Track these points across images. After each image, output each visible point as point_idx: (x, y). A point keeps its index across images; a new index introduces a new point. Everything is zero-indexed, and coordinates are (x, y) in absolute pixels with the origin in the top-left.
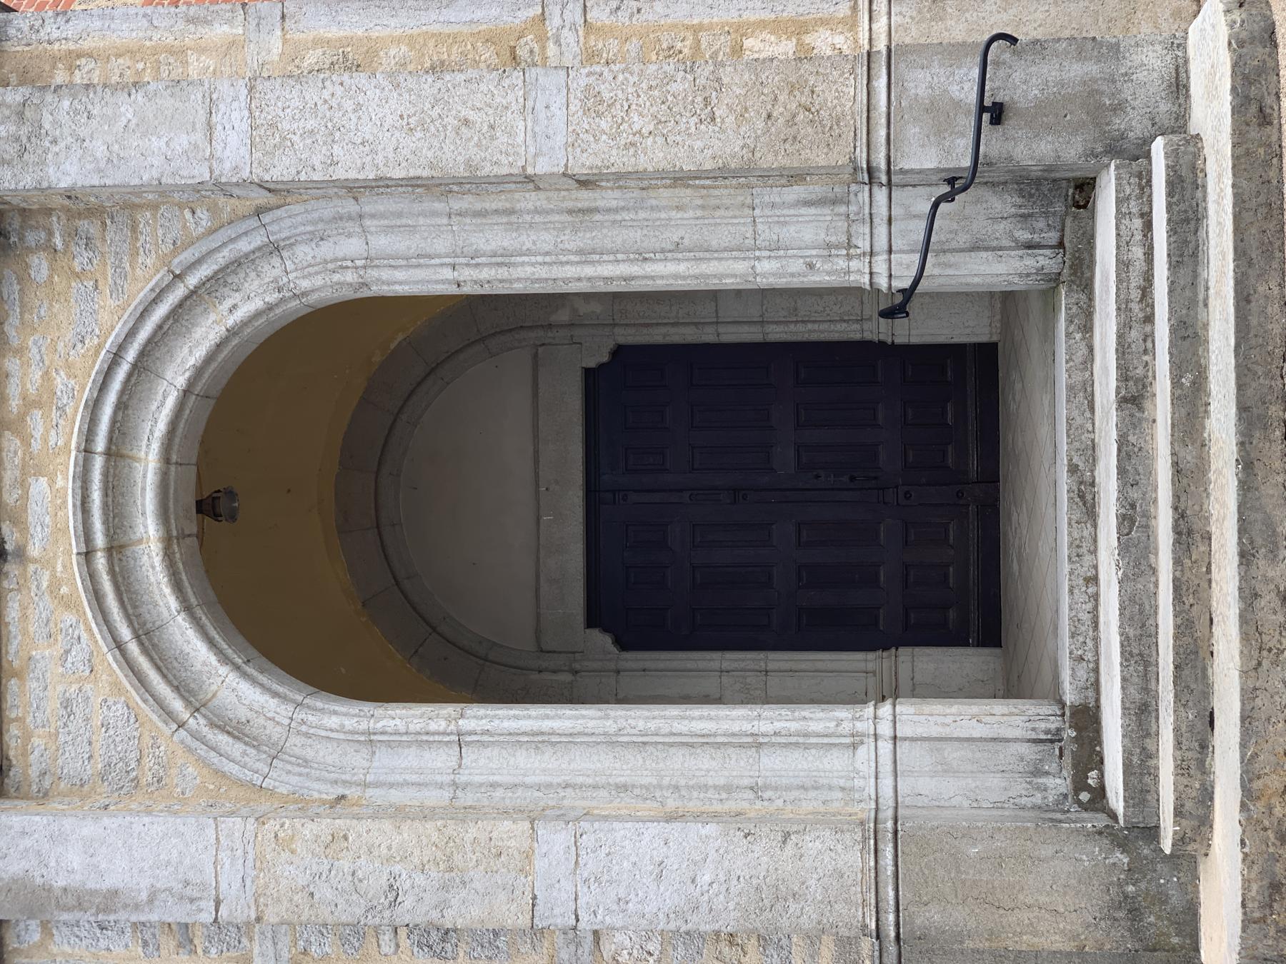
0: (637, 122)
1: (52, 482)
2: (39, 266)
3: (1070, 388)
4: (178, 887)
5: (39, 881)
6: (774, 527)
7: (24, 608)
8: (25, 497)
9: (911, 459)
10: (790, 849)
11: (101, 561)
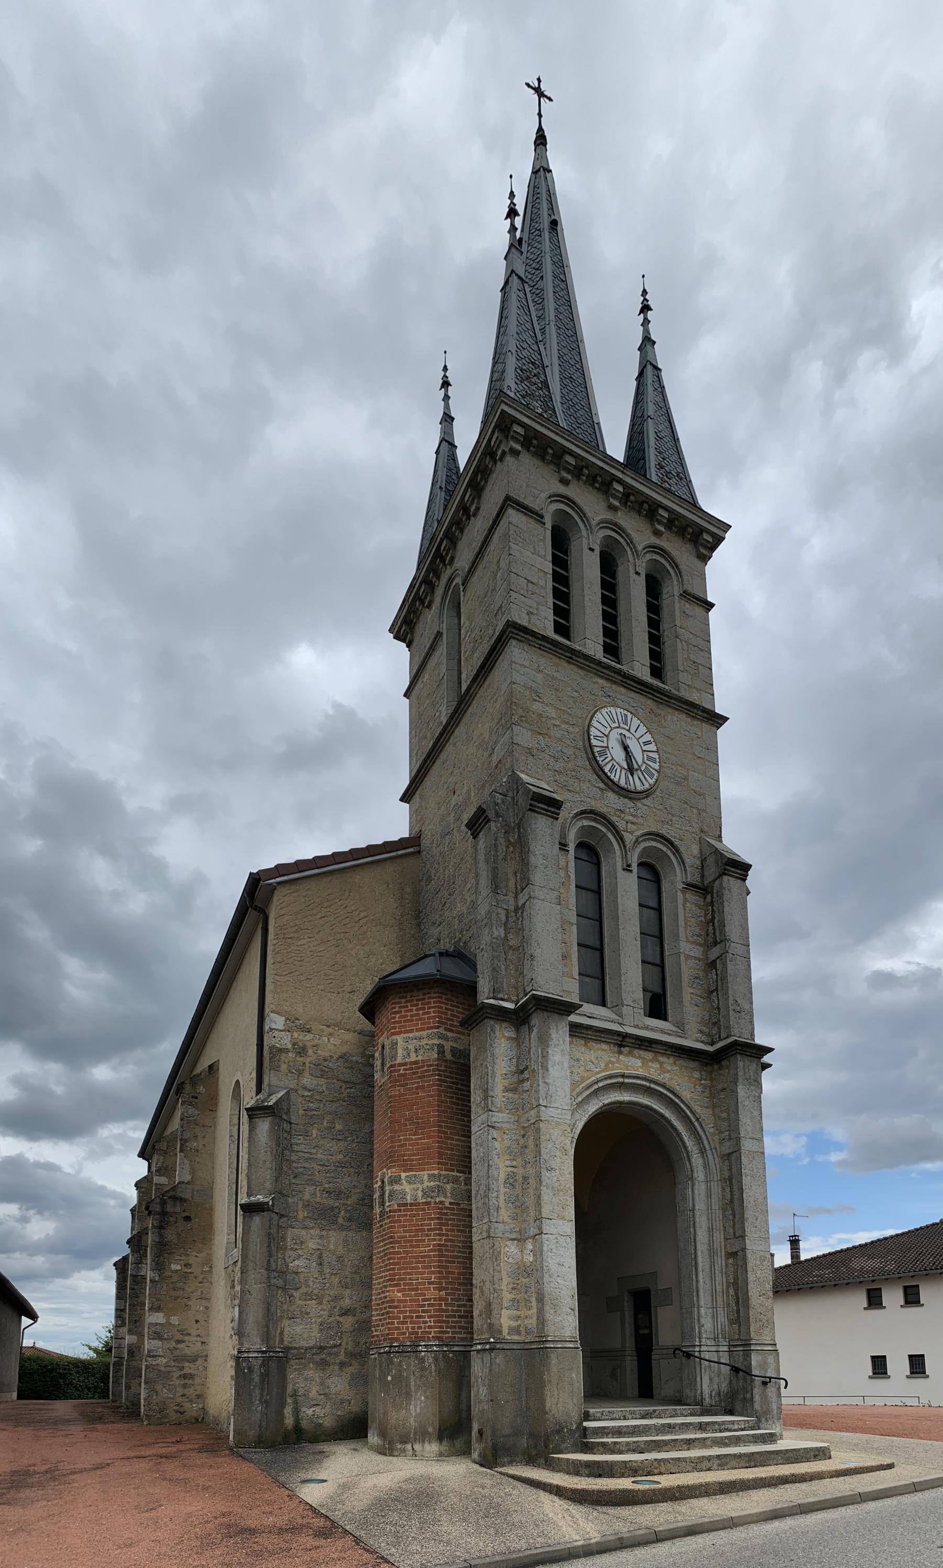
0: (759, 1272)
1: (641, 1067)
2: (696, 1075)
3: (676, 1409)
4: (550, 1093)
5: (550, 1043)
7: (606, 1050)
8: (636, 1057)
10: (569, 1311)
11: (621, 1080)
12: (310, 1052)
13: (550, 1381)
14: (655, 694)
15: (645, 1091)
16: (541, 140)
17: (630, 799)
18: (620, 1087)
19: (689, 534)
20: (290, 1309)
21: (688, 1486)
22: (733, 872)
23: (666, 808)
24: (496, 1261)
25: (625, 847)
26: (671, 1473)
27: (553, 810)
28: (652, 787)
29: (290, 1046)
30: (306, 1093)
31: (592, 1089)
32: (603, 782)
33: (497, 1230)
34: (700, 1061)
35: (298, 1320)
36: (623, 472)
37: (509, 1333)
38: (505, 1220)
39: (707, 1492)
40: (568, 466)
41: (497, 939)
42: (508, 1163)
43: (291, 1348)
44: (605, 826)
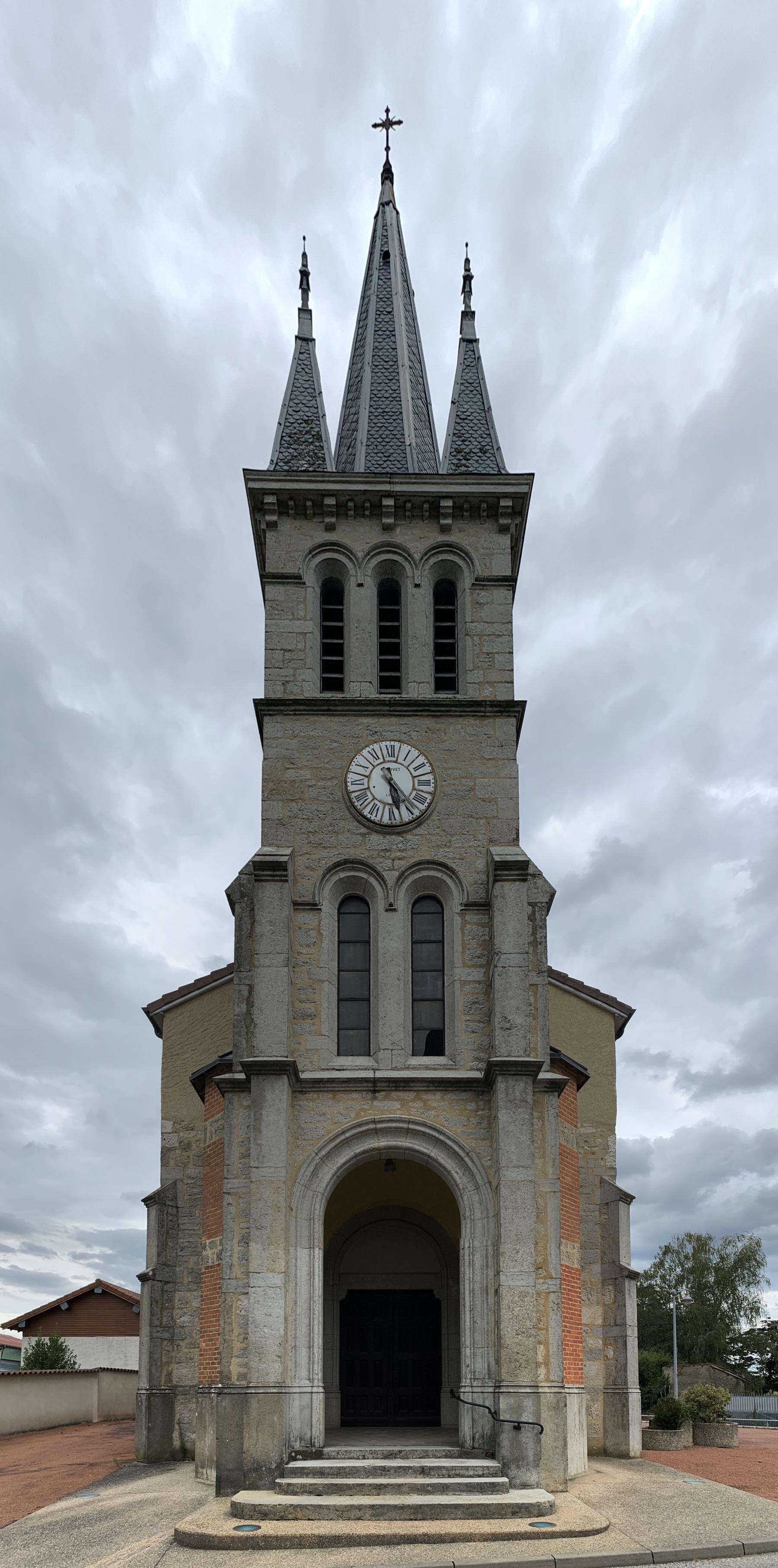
0: (517, 1309)
1: (399, 1109)
2: (472, 1106)
3: (427, 1451)
7: (356, 1099)
8: (394, 1100)
11: (372, 1126)
12: (194, 1146)
13: (249, 1424)
14: (432, 709)
15: (408, 1133)
16: (387, 174)
17: (399, 834)
18: (376, 1133)
19: (484, 511)
20: (178, 1356)
21: (277, 1537)
22: (507, 875)
23: (444, 830)
24: (228, 1314)
25: (386, 886)
26: (309, 1520)
27: (278, 873)
28: (423, 813)
29: (177, 1145)
30: (191, 1181)
31: (338, 1141)
32: (364, 826)
33: (229, 1286)
34: (474, 1091)
35: (184, 1364)
36: (390, 483)
37: (238, 1380)
38: (238, 1276)
39: (300, 1545)
40: (330, 509)
41: (238, 1015)
42: (242, 1225)
43: (179, 1386)
44: (366, 872)
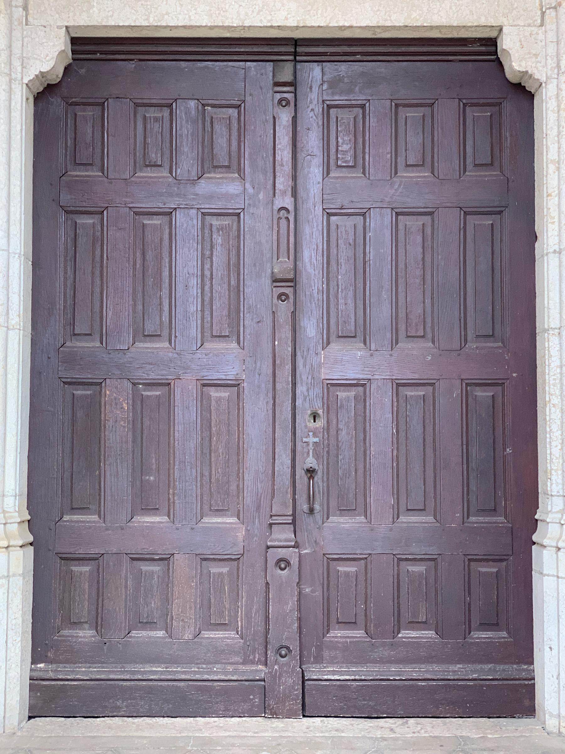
6: (234, 345)
9: (343, 568)
